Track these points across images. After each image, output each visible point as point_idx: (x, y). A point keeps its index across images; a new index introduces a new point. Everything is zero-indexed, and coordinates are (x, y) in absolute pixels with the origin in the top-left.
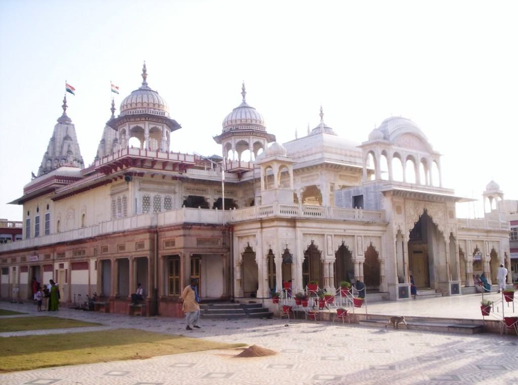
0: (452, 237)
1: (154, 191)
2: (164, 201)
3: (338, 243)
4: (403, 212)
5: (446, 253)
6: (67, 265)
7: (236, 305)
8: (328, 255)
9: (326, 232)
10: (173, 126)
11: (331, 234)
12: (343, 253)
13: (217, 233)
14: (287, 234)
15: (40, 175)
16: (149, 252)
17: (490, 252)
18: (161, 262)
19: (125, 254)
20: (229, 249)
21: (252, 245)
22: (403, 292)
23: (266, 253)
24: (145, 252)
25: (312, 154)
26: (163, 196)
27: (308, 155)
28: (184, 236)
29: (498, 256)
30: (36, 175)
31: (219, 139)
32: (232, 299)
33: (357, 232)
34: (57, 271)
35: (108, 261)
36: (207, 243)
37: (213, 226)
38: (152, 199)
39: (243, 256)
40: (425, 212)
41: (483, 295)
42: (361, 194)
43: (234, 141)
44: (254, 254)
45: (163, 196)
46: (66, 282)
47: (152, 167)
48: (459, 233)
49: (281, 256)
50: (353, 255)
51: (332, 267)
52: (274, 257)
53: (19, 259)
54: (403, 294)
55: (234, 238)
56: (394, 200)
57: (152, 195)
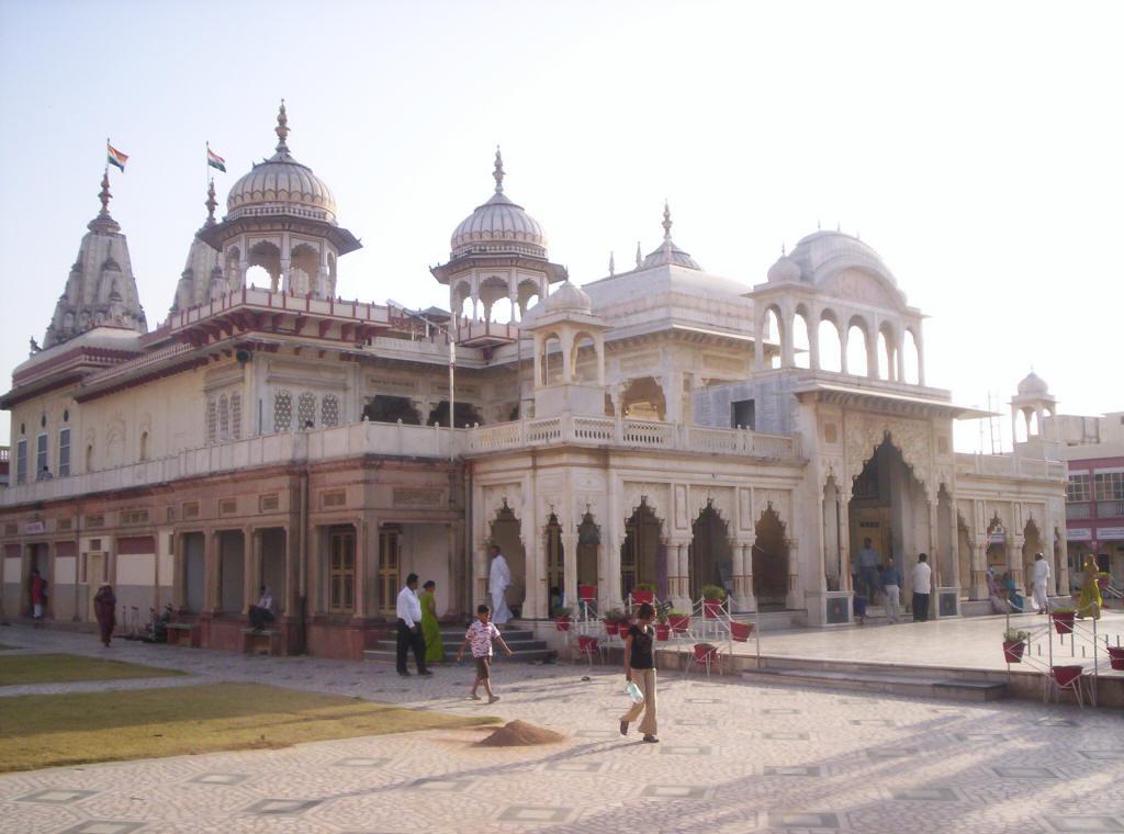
0: (943, 493)
1: (299, 384)
2: (321, 406)
3: (699, 502)
4: (839, 437)
5: (930, 527)
6: (107, 543)
8: (677, 528)
9: (674, 479)
10: (345, 242)
12: (709, 525)
13: (437, 478)
15: (50, 346)
16: (287, 517)
17: (1024, 526)
18: (315, 538)
21: (514, 503)
22: (948, 605)
23: (544, 521)
24: (281, 517)
25: (645, 310)
26: (319, 395)
27: (636, 312)
28: (366, 482)
29: (1041, 536)
30: (40, 345)
33: (741, 478)
34: (85, 555)
35: (199, 536)
37: (427, 463)
38: (295, 403)
39: (493, 528)
40: (888, 438)
42: (749, 398)
43: (475, 279)
44: (517, 523)
45: (319, 395)
47: (296, 333)
48: (960, 484)
49: (575, 529)
50: (730, 530)
51: (685, 553)
54: (836, 614)
55: (474, 488)
57: (296, 393)
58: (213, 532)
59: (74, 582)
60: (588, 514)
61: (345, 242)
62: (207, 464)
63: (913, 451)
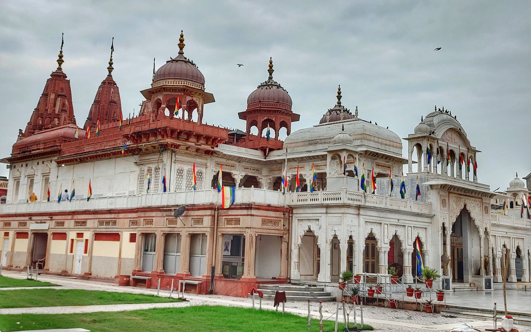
0: (486, 232)
5: (480, 247)
6: (88, 235)
7: (301, 287)
10: (209, 98)
11: (387, 223)
12: (395, 242)
14: (352, 221)
16: (209, 230)
17: (391, 238)
19: (202, 229)
20: (289, 231)
21: (314, 228)
30: (23, 132)
31: (242, 116)
32: (289, 281)
36: (269, 224)
41: (277, 310)
43: (261, 119)
46: (86, 252)
47: (187, 140)
48: (492, 228)
49: (347, 242)
50: (403, 245)
51: (387, 255)
52: (339, 243)
53: (15, 224)
55: (293, 220)
56: (441, 193)
58: (162, 233)
59: (64, 253)
60: (335, 235)
61: (209, 98)
62: (143, 201)
63: (475, 211)
